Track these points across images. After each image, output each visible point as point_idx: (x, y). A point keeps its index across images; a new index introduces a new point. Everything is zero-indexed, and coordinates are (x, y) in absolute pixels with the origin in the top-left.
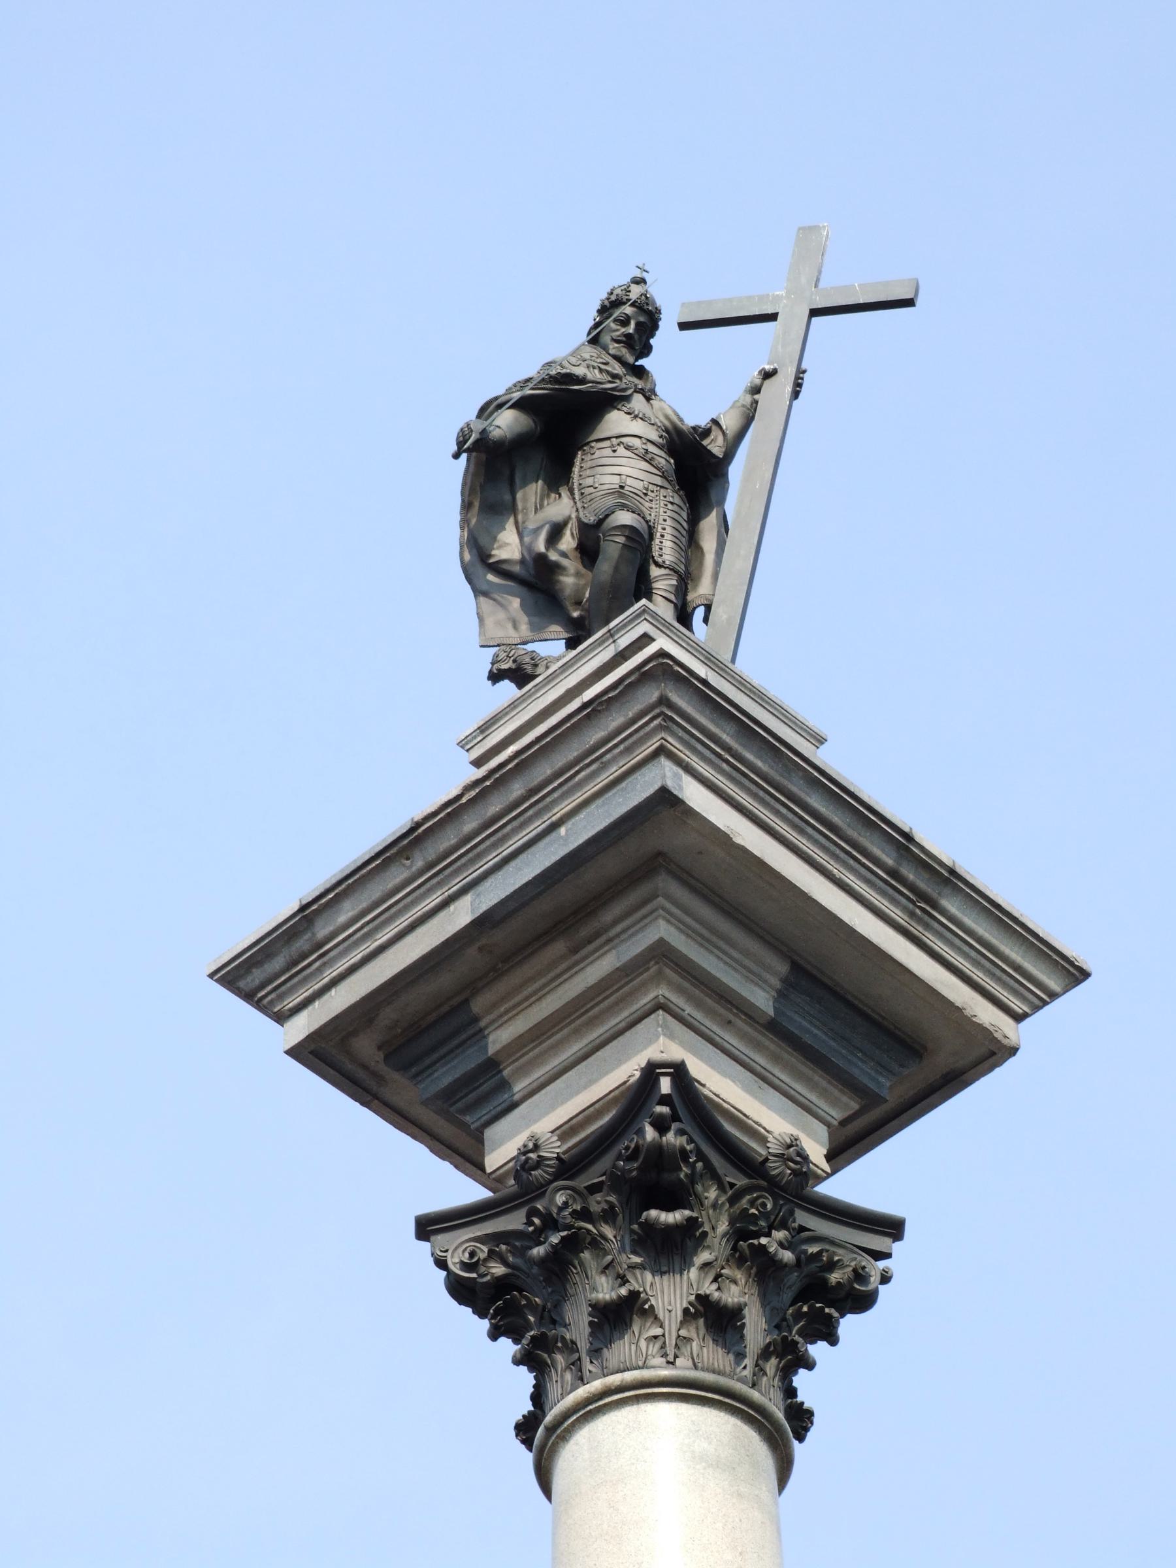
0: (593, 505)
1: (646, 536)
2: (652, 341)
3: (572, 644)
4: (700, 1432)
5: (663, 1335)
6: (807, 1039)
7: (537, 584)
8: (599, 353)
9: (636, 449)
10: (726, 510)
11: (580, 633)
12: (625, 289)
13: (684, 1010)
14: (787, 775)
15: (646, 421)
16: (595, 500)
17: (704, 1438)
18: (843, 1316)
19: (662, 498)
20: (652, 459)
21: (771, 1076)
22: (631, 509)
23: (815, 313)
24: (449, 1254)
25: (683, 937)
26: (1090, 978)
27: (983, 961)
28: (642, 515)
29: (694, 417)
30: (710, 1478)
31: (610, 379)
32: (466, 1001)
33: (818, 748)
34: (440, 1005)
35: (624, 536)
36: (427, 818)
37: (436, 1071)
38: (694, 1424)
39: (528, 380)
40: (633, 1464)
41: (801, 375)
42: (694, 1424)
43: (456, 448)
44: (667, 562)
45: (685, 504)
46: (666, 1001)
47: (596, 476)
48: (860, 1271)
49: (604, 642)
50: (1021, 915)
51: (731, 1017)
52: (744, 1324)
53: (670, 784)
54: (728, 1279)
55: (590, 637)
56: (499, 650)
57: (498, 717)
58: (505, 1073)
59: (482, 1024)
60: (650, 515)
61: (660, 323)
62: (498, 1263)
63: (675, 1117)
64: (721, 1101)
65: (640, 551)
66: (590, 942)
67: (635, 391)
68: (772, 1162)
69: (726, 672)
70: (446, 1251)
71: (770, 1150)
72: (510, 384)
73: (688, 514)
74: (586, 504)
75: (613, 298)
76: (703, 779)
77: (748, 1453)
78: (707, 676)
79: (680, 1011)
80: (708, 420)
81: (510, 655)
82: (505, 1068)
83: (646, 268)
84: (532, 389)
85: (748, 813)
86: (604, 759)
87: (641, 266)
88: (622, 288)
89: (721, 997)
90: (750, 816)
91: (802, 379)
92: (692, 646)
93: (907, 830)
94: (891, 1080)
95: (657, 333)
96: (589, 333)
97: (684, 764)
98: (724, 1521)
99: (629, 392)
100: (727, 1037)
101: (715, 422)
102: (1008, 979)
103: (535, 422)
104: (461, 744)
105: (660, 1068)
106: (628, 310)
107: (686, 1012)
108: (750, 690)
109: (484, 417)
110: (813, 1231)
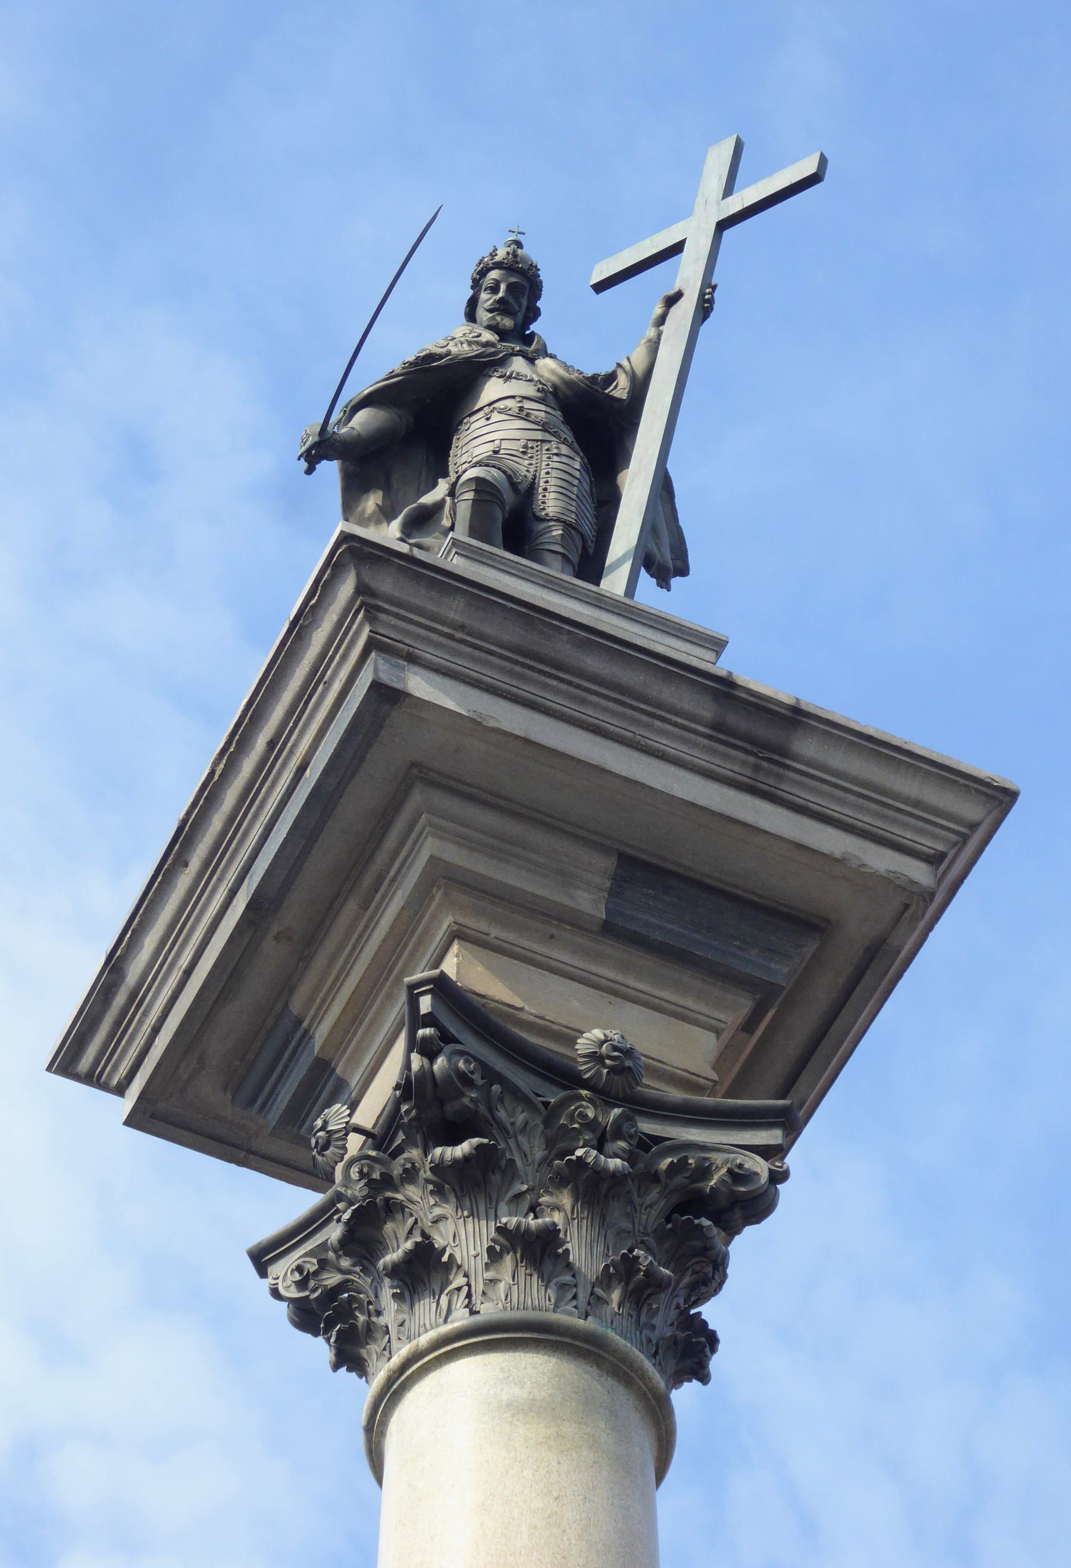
2: (539, 304)
4: (511, 1379)
5: (469, 1285)
6: (657, 936)
9: (510, 409)
13: (488, 934)
15: (521, 379)
17: (516, 1384)
18: (732, 1231)
19: (544, 452)
20: (528, 415)
21: (623, 988)
24: (280, 1281)
25: (465, 852)
26: (1019, 798)
27: (866, 803)
29: (594, 365)
36: (189, 813)
37: (278, 1094)
38: (504, 1371)
42: (504, 1371)
44: (551, 514)
46: (460, 927)
48: (736, 1170)
50: (905, 743)
51: (554, 931)
52: (567, 1251)
53: (385, 678)
54: (548, 1207)
58: (338, 1071)
62: (332, 1272)
63: (446, 1037)
64: (549, 1024)
65: (497, 504)
66: (377, 891)
68: (584, 1064)
69: (564, 587)
70: (278, 1278)
71: (579, 1052)
76: (435, 667)
79: (484, 937)
82: (337, 1065)
86: (326, 678)
89: (533, 911)
90: (509, 696)
92: (523, 572)
94: (788, 965)
97: (404, 654)
98: (535, 1467)
100: (555, 954)
101: (619, 365)
102: (907, 819)
103: (399, 416)
105: (418, 988)
106: (494, 274)
107: (493, 936)
110: (673, 1139)
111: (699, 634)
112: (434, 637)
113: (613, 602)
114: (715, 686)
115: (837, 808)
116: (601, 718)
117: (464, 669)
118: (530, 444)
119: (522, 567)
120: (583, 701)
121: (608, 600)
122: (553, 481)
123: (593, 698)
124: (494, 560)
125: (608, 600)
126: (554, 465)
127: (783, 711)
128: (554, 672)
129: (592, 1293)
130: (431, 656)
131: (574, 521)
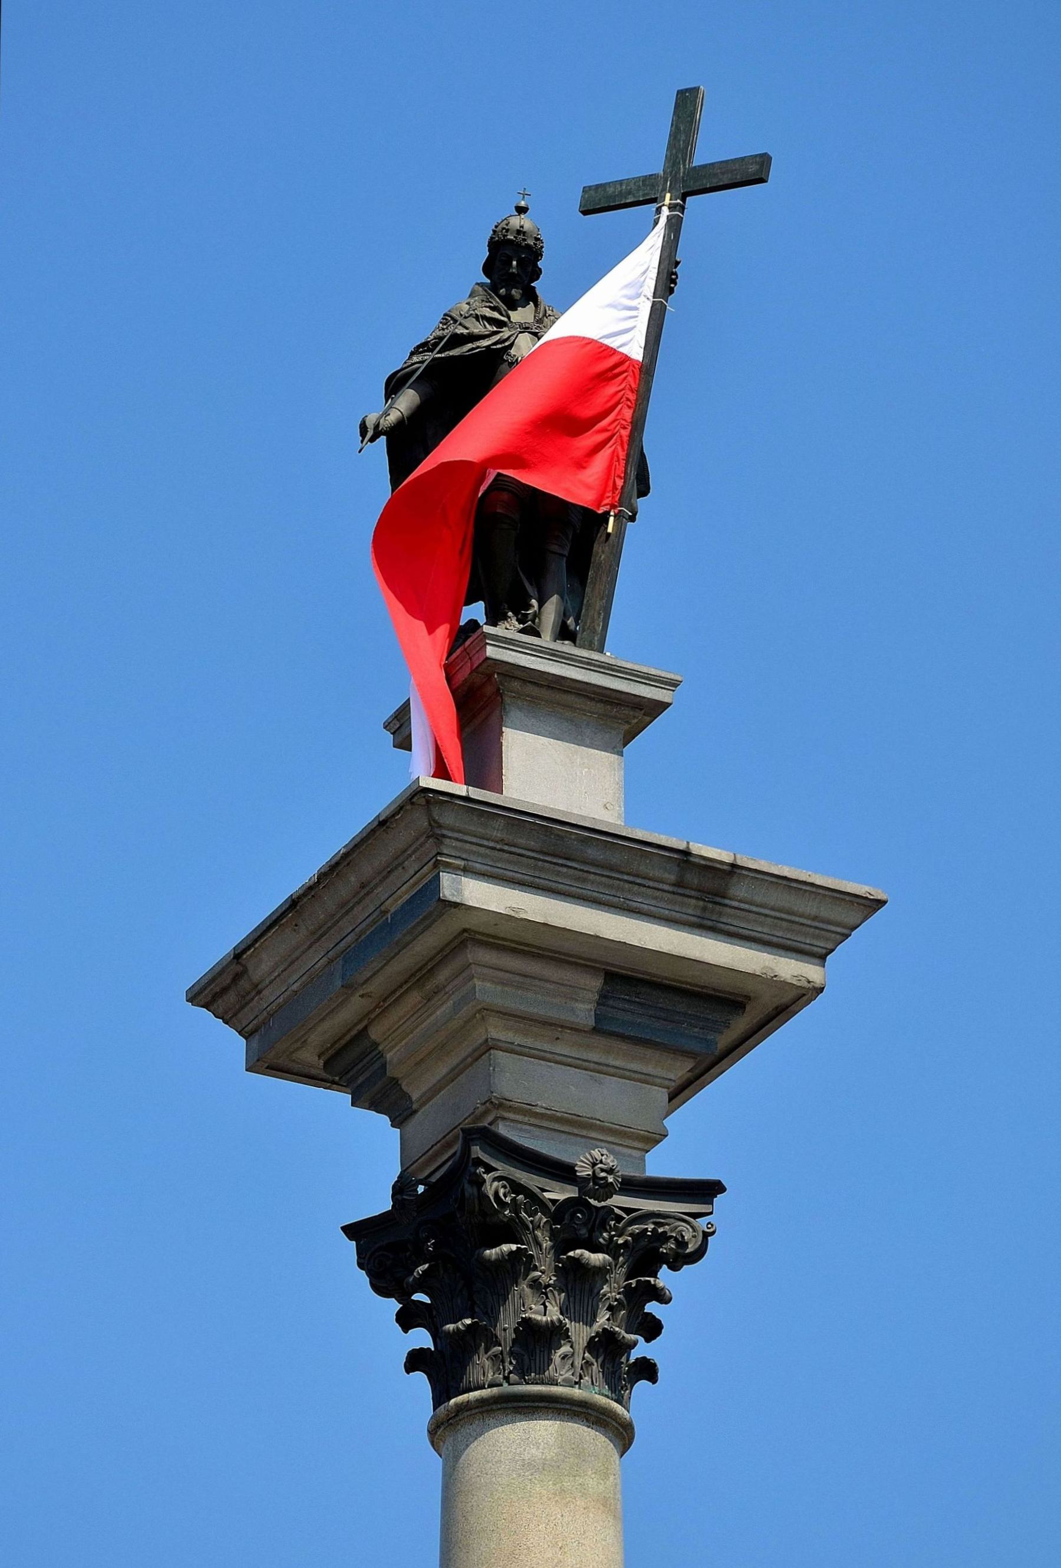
13: (513, 1043)
14: (561, 842)
17: (533, 1445)
30: (536, 1482)
31: (495, 329)
32: (366, 1028)
34: (349, 1030)
40: (478, 1476)
59: (380, 1048)
77: (573, 1446)
92: (535, 650)
97: (462, 867)
108: (599, 666)
112: (482, 850)
115: (760, 929)
119: (534, 647)
120: (585, 880)
123: (592, 877)
124: (514, 645)
127: (725, 867)
129: (584, 1358)
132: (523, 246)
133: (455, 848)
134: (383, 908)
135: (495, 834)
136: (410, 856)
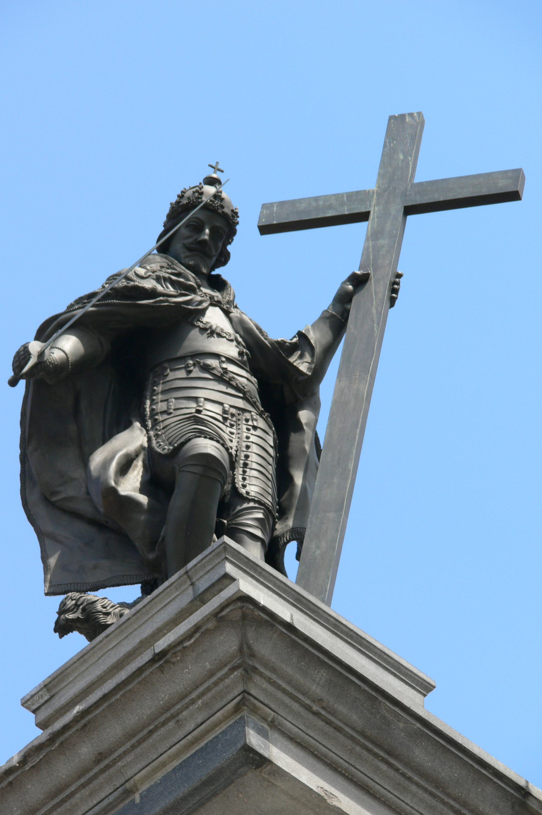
0: (167, 433)
1: (226, 464)
2: (229, 248)
3: (147, 590)
7: (107, 522)
8: (170, 264)
10: (318, 432)
11: (156, 576)
12: (197, 191)
15: (225, 337)
16: (169, 427)
22: (209, 435)
23: (410, 210)
28: (221, 441)
33: (425, 695)
35: (203, 466)
39: (92, 295)
41: (397, 280)
43: (12, 374)
45: (270, 428)
47: (170, 400)
49: (181, 585)
55: (167, 579)
56: (66, 599)
57: (65, 673)
60: (231, 441)
61: (238, 227)
65: (219, 481)
67: (212, 305)
72: (72, 300)
73: (274, 439)
74: (159, 431)
75: (185, 201)
76: (292, 736)
78: (292, 619)
80: (295, 333)
81: (79, 603)
83: (220, 167)
84: (92, 306)
85: (343, 772)
87: (214, 164)
88: (194, 190)
90: (346, 774)
91: (398, 284)
92: (279, 587)
93: (522, 783)
95: (235, 238)
96: (158, 240)
99: (205, 305)
104: (26, 705)
109: (43, 338)
111: (413, 675)
112: (296, 706)
113: (334, 621)
114: (517, 796)
116: (416, 808)
117: (315, 742)
118: (233, 411)
120: (405, 789)
121: (344, 628)
122: (254, 458)
123: (413, 788)
125: (344, 628)
126: (253, 439)
128: (386, 756)
130: (290, 725)
131: (270, 504)
132: (219, 213)
133: (265, 690)
134: (127, 785)
135: (314, 688)
136: (193, 701)
